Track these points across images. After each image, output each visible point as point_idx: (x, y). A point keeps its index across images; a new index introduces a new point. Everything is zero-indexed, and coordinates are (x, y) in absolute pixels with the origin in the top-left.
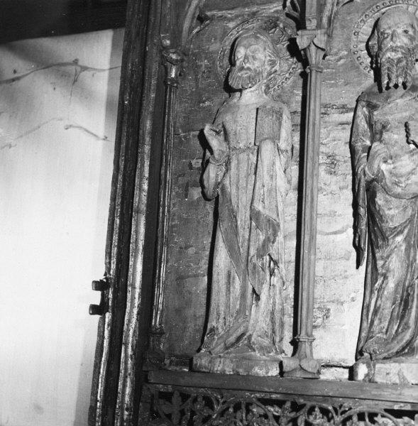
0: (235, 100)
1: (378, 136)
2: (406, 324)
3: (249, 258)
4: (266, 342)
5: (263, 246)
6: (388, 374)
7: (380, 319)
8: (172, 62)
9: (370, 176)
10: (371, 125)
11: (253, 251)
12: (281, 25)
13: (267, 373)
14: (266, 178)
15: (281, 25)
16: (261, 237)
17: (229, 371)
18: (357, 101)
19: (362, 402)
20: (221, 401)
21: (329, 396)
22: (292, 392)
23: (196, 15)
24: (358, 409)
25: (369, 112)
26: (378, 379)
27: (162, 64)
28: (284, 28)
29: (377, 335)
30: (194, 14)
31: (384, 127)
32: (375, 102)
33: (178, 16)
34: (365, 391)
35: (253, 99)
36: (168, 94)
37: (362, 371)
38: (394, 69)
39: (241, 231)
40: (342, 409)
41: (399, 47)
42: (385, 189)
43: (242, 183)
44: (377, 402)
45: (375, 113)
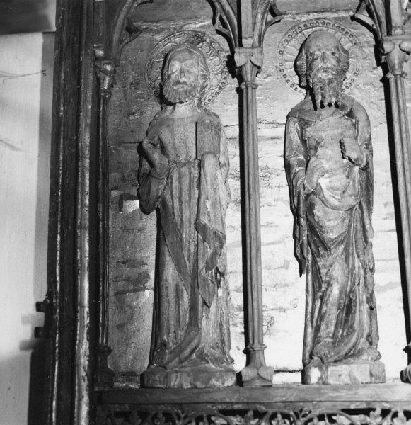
0: (168, 113)
1: (312, 152)
2: (351, 327)
3: (199, 271)
4: (217, 353)
5: (212, 258)
6: (340, 376)
7: (327, 325)
8: (106, 72)
9: (309, 188)
10: (304, 141)
11: (201, 265)
12: (208, 40)
13: (223, 384)
14: (210, 191)
15: (208, 40)
16: (209, 250)
17: (187, 386)
18: (288, 117)
19: (321, 404)
20: (183, 416)
21: (291, 402)
22: (253, 401)
23: (125, 26)
24: (318, 412)
25: (301, 128)
26: (331, 381)
27: (95, 73)
28: (211, 43)
29: (325, 340)
30: (123, 25)
31: (318, 143)
32: (307, 118)
33: (108, 27)
34: (322, 394)
35: (188, 113)
36: (102, 106)
37: (315, 374)
38: (327, 88)
39: (186, 245)
40: (303, 413)
41: (330, 68)
42: (323, 202)
43: (185, 197)
44: (335, 403)
45: (308, 129)
